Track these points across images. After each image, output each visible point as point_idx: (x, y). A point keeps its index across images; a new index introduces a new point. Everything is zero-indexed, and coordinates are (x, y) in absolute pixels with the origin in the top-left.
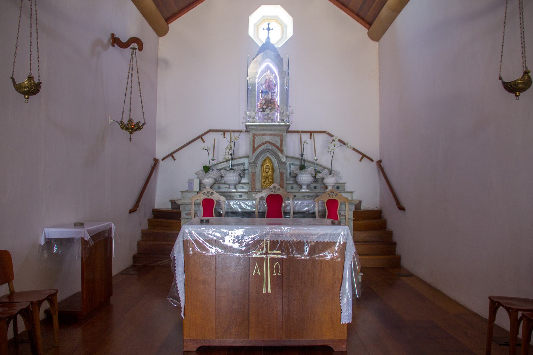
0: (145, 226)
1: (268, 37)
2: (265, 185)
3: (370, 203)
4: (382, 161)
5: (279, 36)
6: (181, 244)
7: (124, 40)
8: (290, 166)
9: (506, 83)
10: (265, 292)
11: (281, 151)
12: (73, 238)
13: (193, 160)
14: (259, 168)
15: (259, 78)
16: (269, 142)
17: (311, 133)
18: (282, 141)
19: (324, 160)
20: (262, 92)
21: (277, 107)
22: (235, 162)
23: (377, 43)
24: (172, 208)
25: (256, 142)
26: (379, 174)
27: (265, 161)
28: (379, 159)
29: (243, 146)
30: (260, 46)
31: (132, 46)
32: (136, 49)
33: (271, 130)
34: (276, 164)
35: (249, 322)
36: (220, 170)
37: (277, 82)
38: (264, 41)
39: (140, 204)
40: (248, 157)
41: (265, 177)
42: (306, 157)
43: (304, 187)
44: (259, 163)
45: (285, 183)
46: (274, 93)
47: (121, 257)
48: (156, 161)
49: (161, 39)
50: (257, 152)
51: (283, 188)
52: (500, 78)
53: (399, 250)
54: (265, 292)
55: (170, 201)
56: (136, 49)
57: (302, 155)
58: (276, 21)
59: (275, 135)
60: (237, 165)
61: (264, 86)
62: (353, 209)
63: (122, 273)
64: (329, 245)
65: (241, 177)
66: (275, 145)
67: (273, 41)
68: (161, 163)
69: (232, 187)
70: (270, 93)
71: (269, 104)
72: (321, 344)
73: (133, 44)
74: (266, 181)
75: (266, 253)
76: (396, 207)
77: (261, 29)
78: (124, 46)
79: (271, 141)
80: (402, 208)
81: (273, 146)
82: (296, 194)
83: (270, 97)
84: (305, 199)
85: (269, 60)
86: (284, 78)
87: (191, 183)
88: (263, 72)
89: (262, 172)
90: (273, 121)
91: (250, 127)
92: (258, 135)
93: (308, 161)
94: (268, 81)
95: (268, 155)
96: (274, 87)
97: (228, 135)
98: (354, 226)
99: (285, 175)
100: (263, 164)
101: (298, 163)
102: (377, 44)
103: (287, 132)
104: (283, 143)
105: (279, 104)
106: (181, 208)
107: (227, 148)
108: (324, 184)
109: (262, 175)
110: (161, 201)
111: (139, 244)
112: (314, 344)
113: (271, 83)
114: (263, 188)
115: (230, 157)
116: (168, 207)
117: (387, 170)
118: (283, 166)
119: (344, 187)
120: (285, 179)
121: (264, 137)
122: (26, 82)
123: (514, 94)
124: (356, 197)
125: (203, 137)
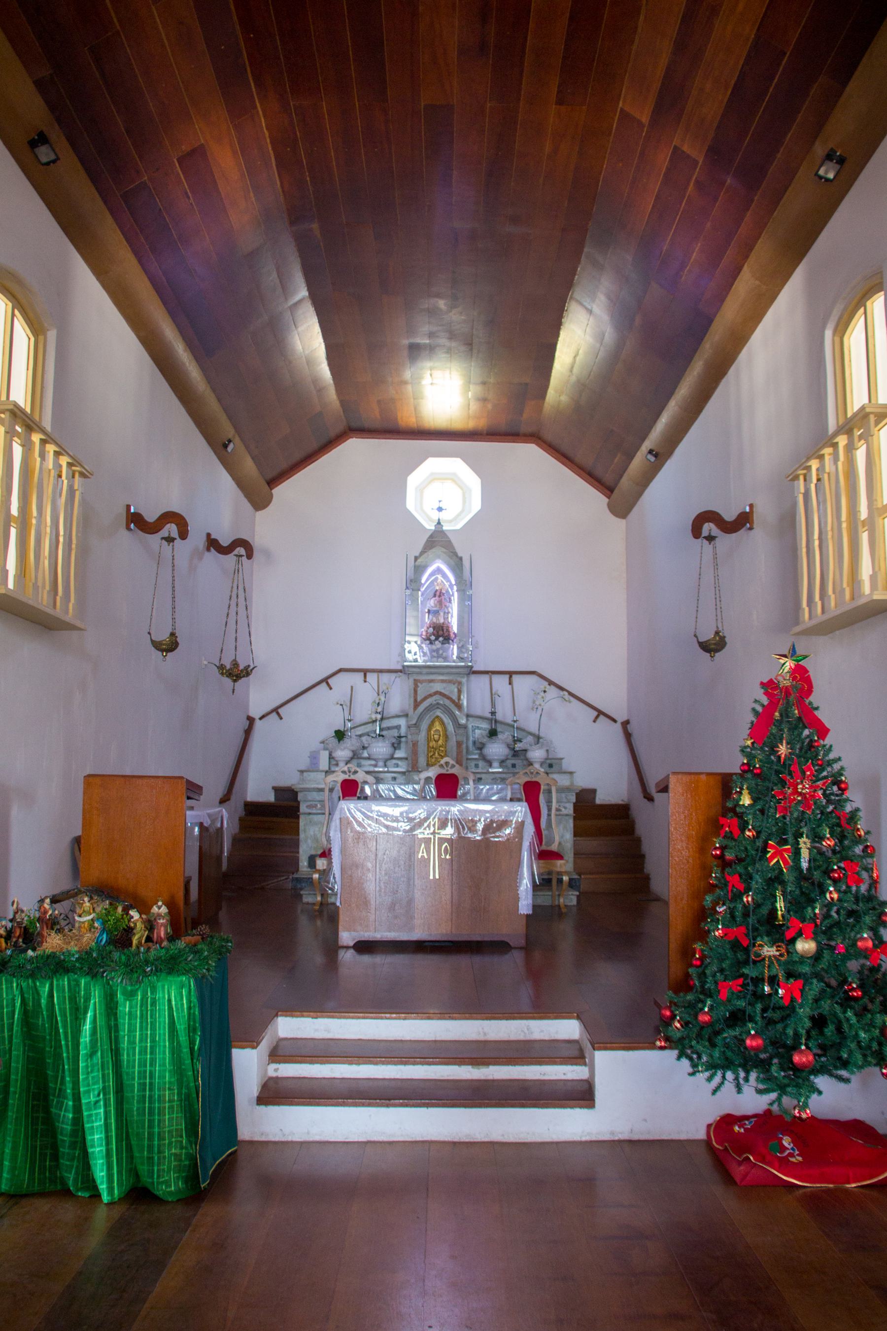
2: (433, 760)
6: (338, 822)
7: (225, 542)
8: (473, 731)
10: (431, 877)
11: (459, 707)
13: (321, 715)
16: (441, 694)
17: (511, 674)
19: (531, 723)
20: (429, 612)
21: (452, 636)
22: (386, 724)
23: (624, 521)
25: (419, 692)
28: (625, 718)
29: (398, 698)
31: (236, 552)
32: (242, 556)
33: (442, 674)
34: (450, 728)
36: (360, 736)
39: (234, 791)
40: (406, 716)
42: (499, 716)
43: (495, 764)
44: (424, 726)
45: (464, 758)
46: (448, 613)
48: (251, 720)
49: (260, 514)
51: (461, 765)
52: (695, 636)
54: (431, 877)
56: (242, 556)
57: (493, 713)
58: (454, 481)
59: (450, 682)
60: (389, 728)
62: (574, 799)
64: (504, 824)
65: (395, 748)
68: (258, 724)
69: (381, 763)
70: (442, 614)
71: (440, 634)
74: (434, 754)
75: (434, 833)
76: (642, 795)
79: (443, 691)
82: (483, 776)
83: (442, 621)
84: (496, 784)
87: (314, 757)
89: (429, 739)
90: (446, 659)
92: (422, 682)
93: (502, 723)
94: (438, 593)
95: (438, 713)
96: (448, 604)
97: (372, 677)
99: (464, 746)
101: (486, 726)
102: (623, 522)
107: (375, 702)
108: (527, 759)
110: (258, 788)
114: (429, 765)
115: (379, 717)
116: (271, 798)
117: (635, 739)
118: (461, 731)
119: (561, 764)
120: (465, 751)
121: (432, 684)
123: (708, 655)
124: (582, 781)
125: (330, 681)
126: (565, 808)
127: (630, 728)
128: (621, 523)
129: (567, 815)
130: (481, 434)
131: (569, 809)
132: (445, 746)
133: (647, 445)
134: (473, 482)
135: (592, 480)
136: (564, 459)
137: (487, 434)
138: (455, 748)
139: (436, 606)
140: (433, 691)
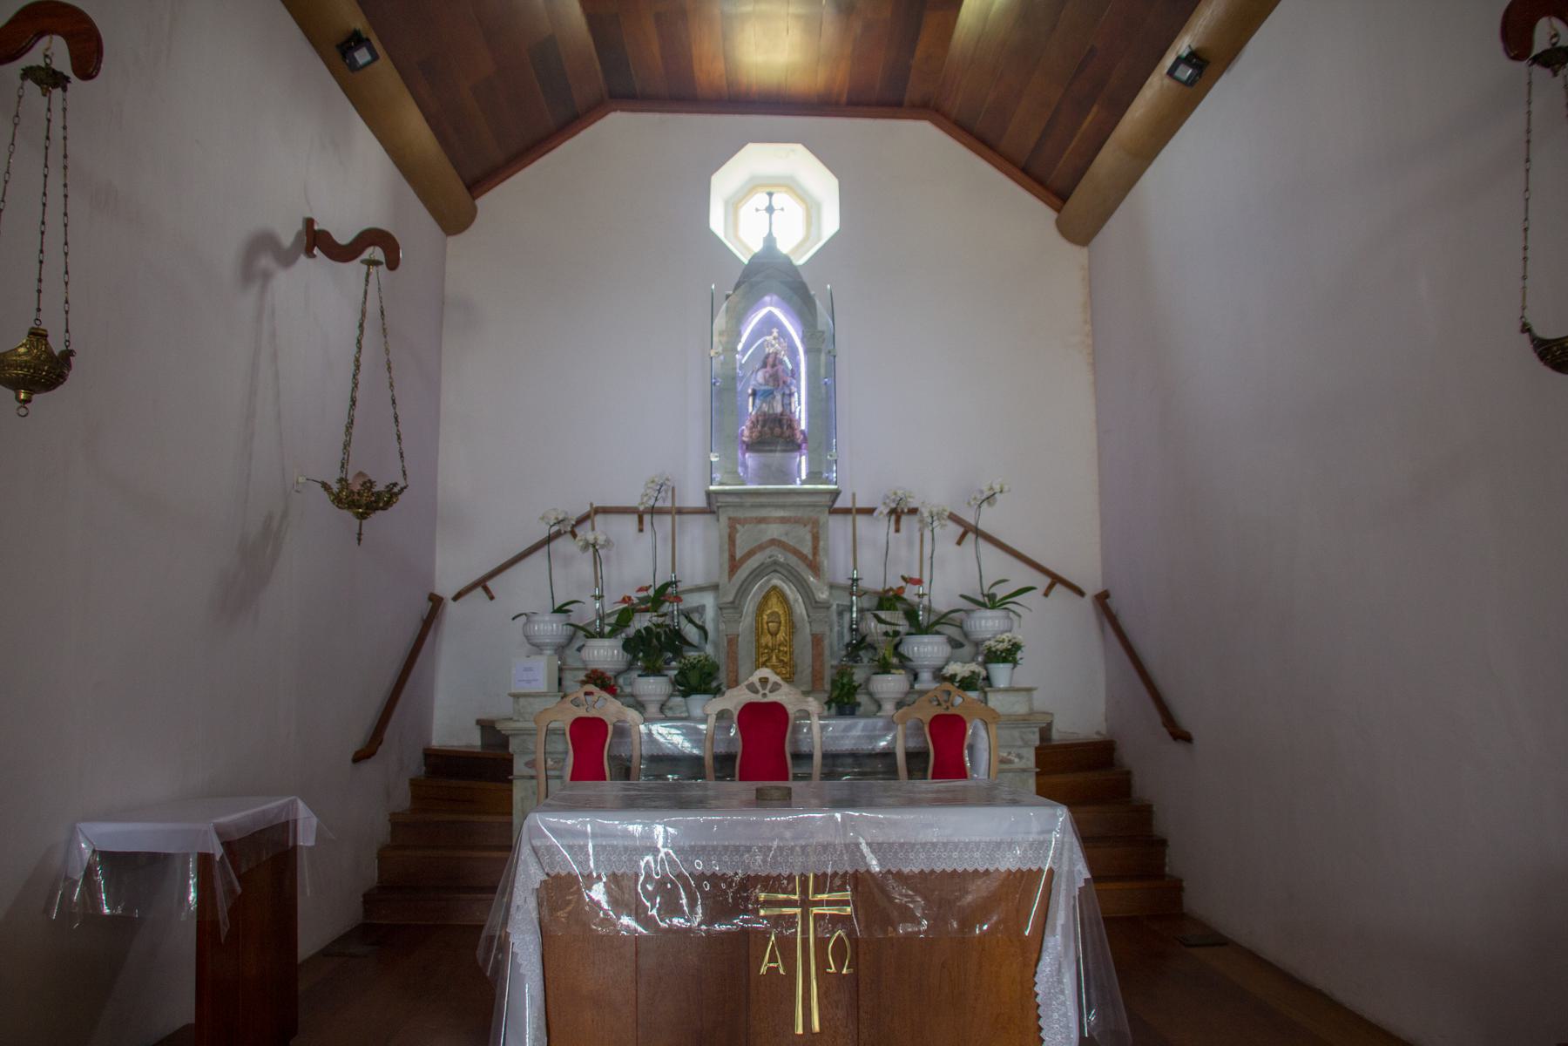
0: (402, 799)
1: (770, 234)
7: (344, 237)
9: (1548, 341)
11: (815, 568)
12: (167, 856)
14: (746, 623)
18: (816, 538)
20: (754, 394)
21: (800, 437)
23: (1085, 251)
24: (483, 746)
25: (738, 542)
27: (766, 598)
28: (1099, 589)
29: (696, 555)
31: (366, 255)
33: (783, 506)
34: (800, 608)
37: (796, 365)
40: (715, 588)
41: (767, 647)
44: (749, 606)
46: (791, 395)
47: (321, 914)
48: (436, 602)
49: (451, 239)
50: (743, 572)
52: (1526, 329)
53: (1175, 862)
54: (800, 1031)
55: (479, 722)
59: (797, 521)
61: (760, 376)
62: (1035, 740)
63: (325, 953)
66: (796, 552)
67: (784, 246)
68: (452, 610)
71: (775, 434)
73: (370, 250)
74: (770, 659)
79: (783, 539)
80: (1181, 736)
83: (779, 409)
85: (775, 298)
86: (819, 351)
88: (757, 333)
89: (758, 633)
91: (721, 499)
92: (744, 522)
94: (771, 360)
95: (776, 582)
96: (789, 380)
99: (826, 642)
100: (760, 609)
104: (821, 543)
105: (803, 426)
110: (451, 723)
111: (382, 857)
116: (471, 740)
117: (1126, 622)
121: (763, 526)
122: (22, 350)
126: (1020, 757)
127: (1112, 603)
128: (1079, 254)
129: (1024, 770)
130: (837, 104)
131: (1029, 759)
132: (790, 642)
134: (823, 184)
139: (767, 383)
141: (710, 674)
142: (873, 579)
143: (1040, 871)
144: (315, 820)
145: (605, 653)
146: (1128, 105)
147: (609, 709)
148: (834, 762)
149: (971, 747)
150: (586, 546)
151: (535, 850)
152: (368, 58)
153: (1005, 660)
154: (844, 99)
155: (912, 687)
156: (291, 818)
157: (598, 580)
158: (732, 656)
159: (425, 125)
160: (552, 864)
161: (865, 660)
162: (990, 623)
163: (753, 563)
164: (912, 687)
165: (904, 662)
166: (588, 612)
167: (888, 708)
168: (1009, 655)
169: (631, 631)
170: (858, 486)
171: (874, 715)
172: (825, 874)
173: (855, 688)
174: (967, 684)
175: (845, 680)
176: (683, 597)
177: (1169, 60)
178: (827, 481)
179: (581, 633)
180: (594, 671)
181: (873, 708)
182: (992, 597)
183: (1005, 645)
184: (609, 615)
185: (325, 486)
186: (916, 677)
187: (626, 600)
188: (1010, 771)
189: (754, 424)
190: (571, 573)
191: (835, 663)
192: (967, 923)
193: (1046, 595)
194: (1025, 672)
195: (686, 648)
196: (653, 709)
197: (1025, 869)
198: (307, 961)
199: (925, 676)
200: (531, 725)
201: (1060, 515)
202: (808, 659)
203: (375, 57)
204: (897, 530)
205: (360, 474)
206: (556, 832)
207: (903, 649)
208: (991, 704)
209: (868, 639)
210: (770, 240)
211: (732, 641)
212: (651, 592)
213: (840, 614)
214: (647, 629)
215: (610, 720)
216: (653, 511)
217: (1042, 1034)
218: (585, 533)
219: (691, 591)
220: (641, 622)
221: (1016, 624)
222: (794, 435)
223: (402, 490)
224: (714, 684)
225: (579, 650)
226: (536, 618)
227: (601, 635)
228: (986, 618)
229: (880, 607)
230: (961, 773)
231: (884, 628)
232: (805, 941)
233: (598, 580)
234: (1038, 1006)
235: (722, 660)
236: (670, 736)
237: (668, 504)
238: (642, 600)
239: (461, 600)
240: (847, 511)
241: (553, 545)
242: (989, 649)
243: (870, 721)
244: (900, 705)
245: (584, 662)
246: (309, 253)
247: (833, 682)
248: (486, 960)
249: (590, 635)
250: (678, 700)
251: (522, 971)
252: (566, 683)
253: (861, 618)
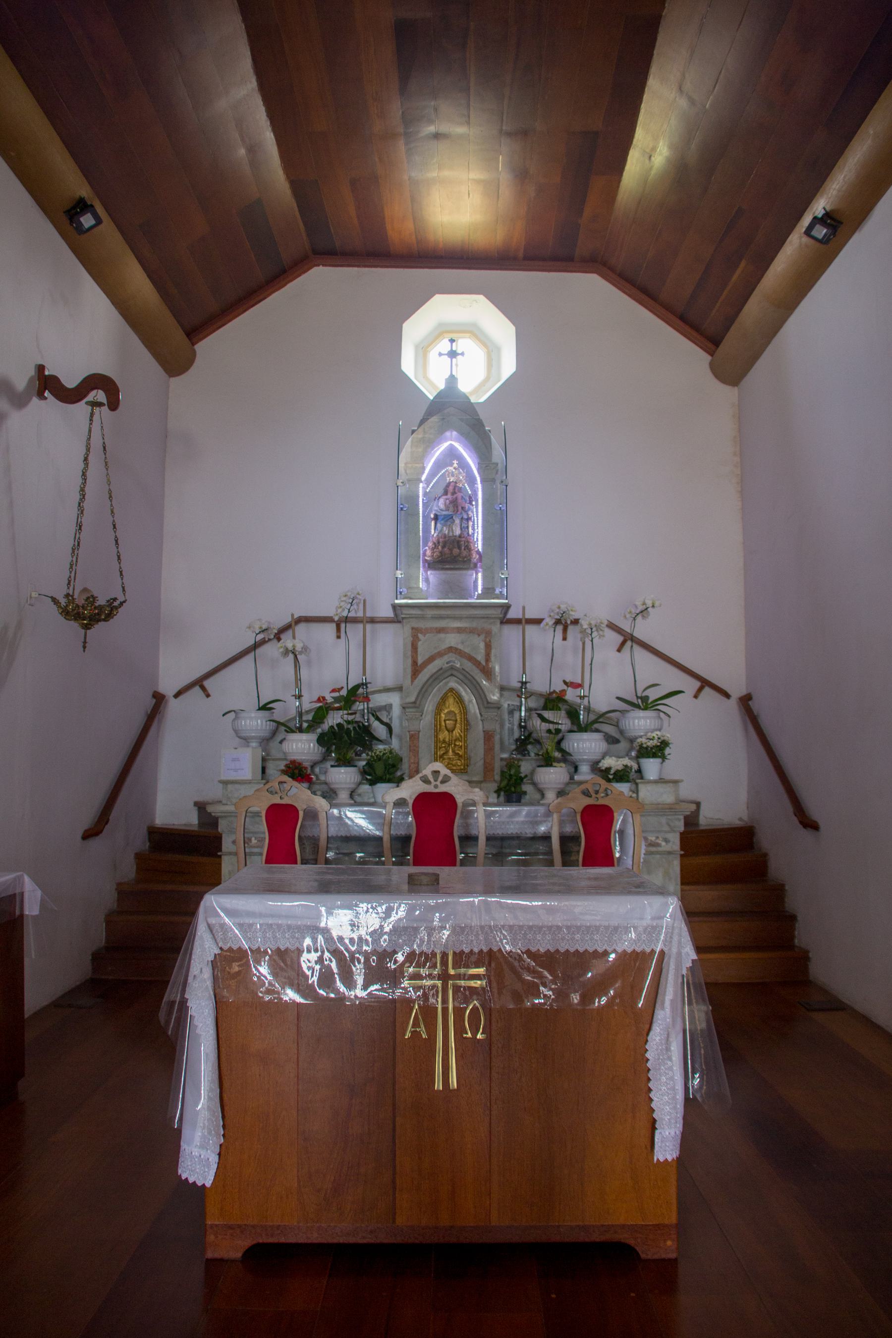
0: (128, 870)
3: (724, 807)
4: (754, 697)
5: (480, 374)
7: (71, 381)
10: (439, 1085)
11: (488, 673)
14: (428, 718)
15: (428, 482)
18: (488, 647)
20: (436, 518)
21: (475, 557)
23: (736, 390)
24: (201, 824)
25: (419, 650)
26: (746, 730)
27: (444, 699)
28: (744, 692)
29: (385, 659)
30: (431, 398)
31: (91, 397)
32: (100, 404)
33: (460, 618)
34: (474, 707)
35: (394, 1174)
37: (475, 492)
38: (442, 386)
40: (399, 689)
41: (444, 741)
44: (429, 706)
46: (468, 519)
48: (159, 699)
53: (803, 937)
55: (196, 804)
56: (100, 404)
59: (472, 631)
61: (441, 503)
66: (471, 659)
67: (465, 386)
68: (173, 706)
70: (457, 521)
71: (452, 555)
72: (603, 1238)
73: (94, 393)
74: (446, 752)
77: (433, 354)
78: (70, 396)
79: (460, 647)
80: (810, 825)
81: (465, 661)
83: (457, 532)
85: (455, 433)
88: (438, 466)
89: (437, 729)
91: (406, 611)
92: (425, 631)
94: (451, 489)
95: (453, 684)
96: (467, 506)
98: (681, 870)
99: (497, 738)
103: (502, 623)
104: (493, 651)
105: (480, 548)
106: (222, 826)
109: (436, 736)
111: (109, 921)
112: (583, 1237)
113: (459, 495)
116: (190, 819)
117: (766, 722)
121: (442, 635)
126: (666, 841)
127: (754, 705)
128: (728, 393)
129: (669, 853)
130: (515, 258)
131: (674, 843)
132: (464, 738)
133: (820, 206)
134: (502, 331)
135: (687, 328)
136: (643, 296)
137: (527, 258)
138: (482, 742)
140: (444, 647)
141: (394, 766)
142: (540, 684)
143: (653, 952)
144: (39, 893)
145: (302, 746)
146: (772, 259)
147: (299, 795)
148: (501, 846)
149: (622, 832)
150: (286, 652)
151: (210, 928)
152: (92, 222)
153: (654, 756)
154: (521, 254)
155: (572, 778)
156: (17, 891)
157: (298, 680)
158: (414, 750)
159: (147, 280)
160: (225, 940)
161: (532, 754)
162: (642, 722)
163: (438, 664)
164: (572, 778)
165: (566, 757)
166: (288, 709)
167: (550, 796)
168: (658, 750)
169: (325, 727)
170: (528, 599)
171: (537, 803)
172: (462, 952)
173: (522, 779)
174: (621, 776)
175: (512, 772)
176: (370, 696)
177: (807, 220)
178: (500, 596)
179: (283, 728)
180: (293, 762)
181: (537, 796)
182: (645, 699)
183: (655, 742)
184: (308, 712)
185: (55, 600)
186: (576, 769)
187: (321, 699)
188: (657, 853)
189: (436, 545)
190: (274, 677)
191: (505, 756)
192: (587, 998)
193: (696, 697)
194: (675, 764)
195: (375, 742)
196: (343, 796)
197: (638, 950)
198: (39, 1014)
199: (584, 768)
200: (231, 808)
201: (709, 628)
202: (481, 751)
203: (99, 221)
204: (565, 639)
205: (85, 590)
206: (230, 913)
207: (565, 745)
208: (642, 794)
209: (534, 735)
210: (452, 380)
211: (414, 737)
212: (344, 693)
213: (511, 712)
214: (339, 725)
215: (301, 807)
216: (347, 620)
217: (652, 1095)
218: (288, 641)
219: (380, 691)
220: (334, 719)
221: (666, 724)
222: (470, 555)
223: (122, 604)
224: (399, 774)
225: (281, 742)
226: (243, 714)
227: (300, 730)
228: (639, 718)
229: (545, 708)
230: (608, 860)
231: (545, 726)
232: (445, 1010)
233: (298, 680)
234: (649, 1070)
235: (404, 753)
236: (358, 820)
237: (360, 614)
238: (337, 699)
239: (181, 697)
240: (518, 621)
241: (259, 651)
242: (641, 746)
243: (533, 808)
244: (561, 793)
245: (285, 753)
246: (41, 395)
247: (502, 772)
248: (168, 1022)
249: (291, 731)
250: (366, 787)
251: (198, 1031)
252: (268, 771)
253: (529, 717)
